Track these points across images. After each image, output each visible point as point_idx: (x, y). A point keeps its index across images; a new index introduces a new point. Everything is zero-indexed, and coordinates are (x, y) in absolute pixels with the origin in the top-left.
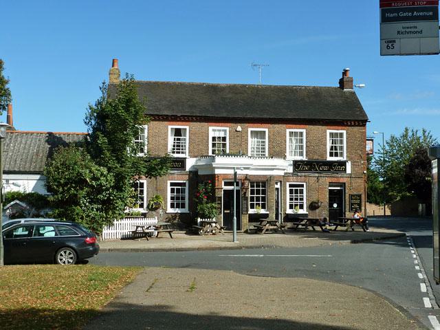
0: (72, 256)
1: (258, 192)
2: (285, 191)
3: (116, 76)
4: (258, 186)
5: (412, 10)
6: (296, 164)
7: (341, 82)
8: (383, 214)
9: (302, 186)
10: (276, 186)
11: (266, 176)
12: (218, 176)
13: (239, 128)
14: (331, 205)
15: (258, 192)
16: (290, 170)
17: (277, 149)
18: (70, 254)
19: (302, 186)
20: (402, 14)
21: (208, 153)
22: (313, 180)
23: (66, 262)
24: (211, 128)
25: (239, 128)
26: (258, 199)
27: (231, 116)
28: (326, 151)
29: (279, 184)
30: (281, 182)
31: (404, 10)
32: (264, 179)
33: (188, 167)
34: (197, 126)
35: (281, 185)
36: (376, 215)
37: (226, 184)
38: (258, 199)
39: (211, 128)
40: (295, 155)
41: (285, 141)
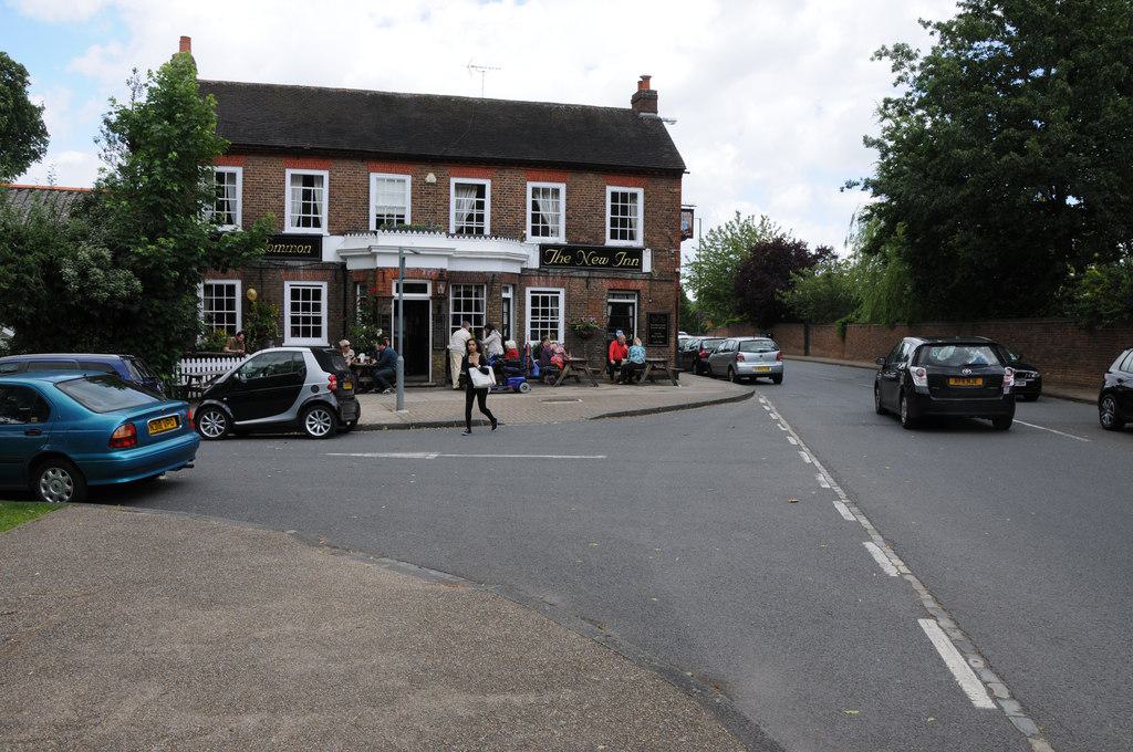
2: (522, 304)
4: (468, 294)
7: (636, 100)
10: (504, 295)
13: (431, 178)
17: (508, 222)
24: (374, 177)
25: (431, 178)
29: (511, 290)
30: (514, 286)
35: (514, 294)
39: (374, 177)
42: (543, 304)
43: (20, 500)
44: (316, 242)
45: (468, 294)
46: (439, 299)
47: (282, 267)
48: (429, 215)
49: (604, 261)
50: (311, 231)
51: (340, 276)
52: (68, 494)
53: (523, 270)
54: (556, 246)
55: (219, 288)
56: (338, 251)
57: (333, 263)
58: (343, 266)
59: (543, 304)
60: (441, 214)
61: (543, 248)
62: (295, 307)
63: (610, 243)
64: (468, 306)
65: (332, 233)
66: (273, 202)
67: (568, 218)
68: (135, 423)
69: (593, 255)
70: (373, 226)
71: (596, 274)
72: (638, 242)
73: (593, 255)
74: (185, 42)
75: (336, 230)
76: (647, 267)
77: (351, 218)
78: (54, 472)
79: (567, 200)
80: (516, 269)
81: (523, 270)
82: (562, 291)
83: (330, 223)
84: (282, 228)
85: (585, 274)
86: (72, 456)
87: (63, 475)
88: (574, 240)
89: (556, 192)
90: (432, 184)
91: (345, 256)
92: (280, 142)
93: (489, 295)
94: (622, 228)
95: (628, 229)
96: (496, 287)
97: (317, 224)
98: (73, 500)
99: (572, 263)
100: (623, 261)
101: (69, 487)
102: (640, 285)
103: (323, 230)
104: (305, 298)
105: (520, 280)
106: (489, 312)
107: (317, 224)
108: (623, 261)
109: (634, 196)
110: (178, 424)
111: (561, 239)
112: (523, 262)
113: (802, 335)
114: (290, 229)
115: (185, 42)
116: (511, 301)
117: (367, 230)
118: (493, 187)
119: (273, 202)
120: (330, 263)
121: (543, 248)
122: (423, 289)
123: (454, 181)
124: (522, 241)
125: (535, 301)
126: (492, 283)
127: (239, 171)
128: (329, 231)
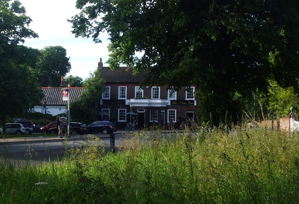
30: (165, 109)
37: (139, 110)
39: (136, 87)
42: (172, 113)
46: (147, 113)
48: (147, 96)
49: (185, 103)
50: (123, 99)
53: (167, 106)
54: (174, 100)
55: (172, 111)
61: (171, 101)
62: (170, 114)
63: (187, 99)
64: (154, 114)
69: (182, 102)
70: (152, 98)
71: (183, 106)
72: (194, 99)
73: (182, 102)
74: (101, 59)
76: (195, 104)
77: (131, 96)
80: (165, 106)
81: (167, 106)
82: (176, 111)
84: (118, 98)
85: (181, 106)
92: (117, 81)
94: (190, 96)
95: (157, 91)
97: (125, 97)
99: (178, 104)
100: (189, 103)
102: (194, 108)
103: (126, 98)
107: (125, 97)
108: (189, 103)
111: (176, 99)
113: (289, 120)
114: (119, 98)
115: (101, 59)
121: (171, 101)
122: (142, 110)
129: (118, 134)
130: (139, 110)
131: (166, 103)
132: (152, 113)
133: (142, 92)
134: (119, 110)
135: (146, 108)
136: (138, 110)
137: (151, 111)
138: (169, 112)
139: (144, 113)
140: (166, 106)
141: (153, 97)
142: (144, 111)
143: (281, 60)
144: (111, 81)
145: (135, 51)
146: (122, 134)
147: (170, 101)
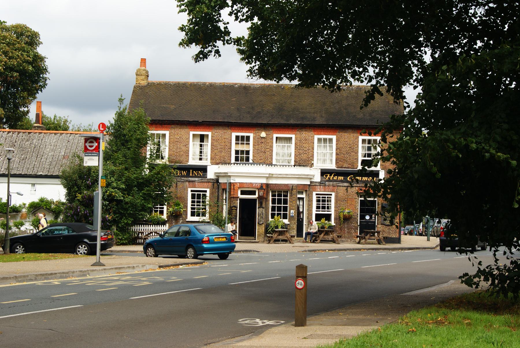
0: (86, 248)
1: (279, 202)
2: (310, 201)
3: (143, 77)
4: (279, 195)
5: (91, 153)
6: (324, 173)
8: (7, 184)
9: (206, 191)
11: (251, 184)
12: (234, 184)
14: (362, 217)
15: (279, 202)
16: (318, 178)
17: (304, 157)
18: (85, 247)
19: (206, 191)
20: (89, 154)
21: (230, 160)
22: (342, 191)
23: (83, 253)
25: (263, 134)
26: (279, 209)
27: (254, 121)
28: (357, 159)
30: (306, 191)
31: (90, 153)
32: (285, 189)
33: (211, 175)
34: (220, 132)
36: (7, 182)
37: (243, 193)
38: (279, 209)
40: (323, 164)
41: (313, 148)
42: (323, 202)
43: (53, 253)
44: (204, 169)
45: (279, 195)
47: (187, 181)
51: (216, 185)
52: (153, 255)
56: (215, 173)
57: (213, 179)
58: (217, 181)
59: (323, 202)
60: (268, 153)
65: (212, 163)
66: (184, 148)
67: (337, 154)
68: (209, 237)
74: (143, 61)
75: (215, 162)
78: (151, 249)
79: (336, 144)
82: (333, 194)
83: (212, 159)
84: (188, 161)
86: (194, 245)
87: (153, 250)
88: (340, 166)
89: (331, 140)
90: (264, 138)
91: (218, 176)
92: (292, 122)
93: (291, 196)
96: (294, 191)
98: (154, 257)
101: (193, 256)
104: (198, 197)
105: (307, 189)
106: (290, 205)
109: (164, 135)
110: (226, 240)
112: (311, 179)
116: (305, 199)
117: (230, 163)
118: (296, 139)
119: (184, 148)
120: (210, 179)
122: (253, 193)
123: (275, 136)
124: (311, 167)
125: (193, 196)
126: (292, 189)
127: (167, 133)
128: (211, 163)
129: (345, 250)
130: (241, 191)
131: (311, 175)
132: (274, 201)
133: (236, 144)
134: (189, 190)
135: (261, 187)
136: (239, 192)
137: (272, 196)
138: (192, 198)
139: (255, 200)
140: (309, 183)
141: (237, 159)
142: (255, 194)
143: (212, 2)
144: (358, 123)
145: (246, 38)
146: (327, 251)
147: (320, 171)
